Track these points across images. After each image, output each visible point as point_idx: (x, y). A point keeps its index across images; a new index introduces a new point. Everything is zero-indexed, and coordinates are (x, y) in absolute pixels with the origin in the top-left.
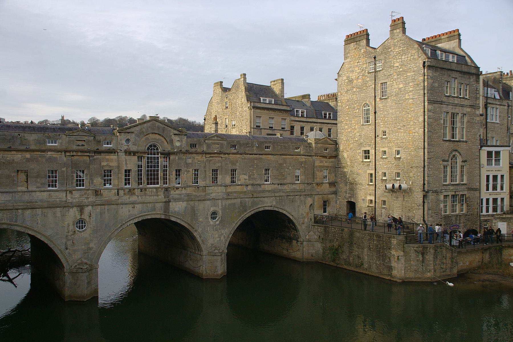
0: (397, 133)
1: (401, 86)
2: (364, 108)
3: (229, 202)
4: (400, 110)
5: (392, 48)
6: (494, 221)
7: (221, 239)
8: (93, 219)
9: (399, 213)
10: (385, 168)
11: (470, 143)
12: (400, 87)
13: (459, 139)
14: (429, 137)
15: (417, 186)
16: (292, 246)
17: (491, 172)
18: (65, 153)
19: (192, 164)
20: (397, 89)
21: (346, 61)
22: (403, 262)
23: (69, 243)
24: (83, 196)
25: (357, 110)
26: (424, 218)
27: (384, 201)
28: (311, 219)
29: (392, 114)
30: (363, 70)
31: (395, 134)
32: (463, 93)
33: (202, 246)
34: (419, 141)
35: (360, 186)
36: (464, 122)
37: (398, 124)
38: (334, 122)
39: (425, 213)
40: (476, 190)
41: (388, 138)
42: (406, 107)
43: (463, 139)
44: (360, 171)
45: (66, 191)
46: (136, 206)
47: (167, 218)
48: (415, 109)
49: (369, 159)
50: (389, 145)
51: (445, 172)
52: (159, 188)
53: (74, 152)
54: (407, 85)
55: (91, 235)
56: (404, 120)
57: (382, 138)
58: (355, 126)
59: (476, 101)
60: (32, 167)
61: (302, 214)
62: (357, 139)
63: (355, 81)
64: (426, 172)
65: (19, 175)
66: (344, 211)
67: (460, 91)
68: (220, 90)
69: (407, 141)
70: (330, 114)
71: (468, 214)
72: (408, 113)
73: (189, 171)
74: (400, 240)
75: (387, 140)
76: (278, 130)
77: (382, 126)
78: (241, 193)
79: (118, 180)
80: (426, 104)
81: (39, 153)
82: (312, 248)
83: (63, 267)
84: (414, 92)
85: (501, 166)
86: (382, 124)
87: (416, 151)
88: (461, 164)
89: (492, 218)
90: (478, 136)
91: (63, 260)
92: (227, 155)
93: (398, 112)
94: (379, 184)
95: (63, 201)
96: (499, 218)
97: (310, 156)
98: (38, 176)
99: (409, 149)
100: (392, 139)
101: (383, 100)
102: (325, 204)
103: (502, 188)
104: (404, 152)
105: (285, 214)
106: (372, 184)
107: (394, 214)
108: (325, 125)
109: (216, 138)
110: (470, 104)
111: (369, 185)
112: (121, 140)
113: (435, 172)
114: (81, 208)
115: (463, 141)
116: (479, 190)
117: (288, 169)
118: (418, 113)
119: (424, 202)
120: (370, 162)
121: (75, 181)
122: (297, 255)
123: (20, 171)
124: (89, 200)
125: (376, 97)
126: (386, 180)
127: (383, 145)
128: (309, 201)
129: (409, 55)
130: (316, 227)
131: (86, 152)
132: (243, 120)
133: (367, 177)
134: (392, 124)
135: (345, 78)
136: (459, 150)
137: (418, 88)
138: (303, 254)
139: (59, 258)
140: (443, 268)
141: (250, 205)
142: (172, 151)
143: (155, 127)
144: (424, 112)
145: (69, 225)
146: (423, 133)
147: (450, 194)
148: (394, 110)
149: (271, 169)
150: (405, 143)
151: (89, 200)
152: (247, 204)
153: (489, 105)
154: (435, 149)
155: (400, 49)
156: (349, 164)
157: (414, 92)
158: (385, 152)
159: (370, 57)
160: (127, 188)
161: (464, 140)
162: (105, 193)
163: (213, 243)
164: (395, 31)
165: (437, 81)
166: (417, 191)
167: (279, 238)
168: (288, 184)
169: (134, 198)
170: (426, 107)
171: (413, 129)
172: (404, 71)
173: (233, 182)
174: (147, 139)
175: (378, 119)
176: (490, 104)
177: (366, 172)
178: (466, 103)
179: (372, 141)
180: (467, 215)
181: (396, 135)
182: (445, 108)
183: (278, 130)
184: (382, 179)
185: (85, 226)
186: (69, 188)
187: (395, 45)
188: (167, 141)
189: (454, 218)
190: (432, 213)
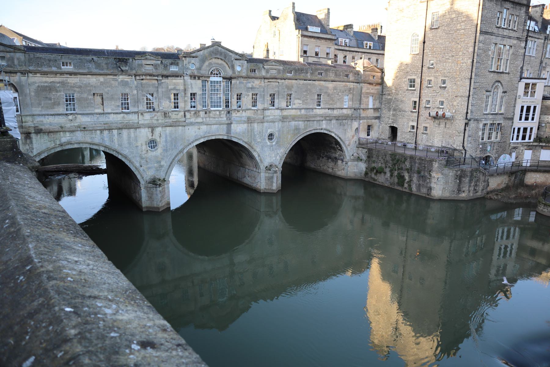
0: (445, 62)
2: (413, 38)
4: (450, 40)
6: (522, 148)
7: (277, 158)
8: (163, 139)
9: (440, 138)
10: (430, 97)
11: (511, 74)
12: (452, 17)
13: (503, 70)
14: (477, 68)
15: (460, 114)
16: (337, 165)
17: (533, 103)
18: (135, 77)
19: (251, 88)
20: (449, 20)
22: (442, 183)
23: (143, 162)
24: (153, 118)
26: (463, 143)
27: (426, 127)
28: (356, 142)
29: (442, 44)
31: (442, 64)
32: (512, 24)
34: (466, 71)
35: (403, 112)
37: (446, 54)
38: (381, 52)
39: (465, 140)
41: (435, 68)
42: (457, 38)
43: (506, 70)
44: (404, 99)
46: (201, 127)
47: (229, 139)
48: (466, 40)
49: (414, 87)
50: (435, 74)
51: (487, 102)
52: (221, 111)
53: (143, 76)
54: (460, 15)
55: (162, 154)
56: (453, 51)
57: (429, 68)
59: (523, 33)
60: (106, 90)
62: (403, 68)
64: (471, 101)
65: (95, 98)
66: (387, 133)
67: (510, 23)
69: (454, 71)
71: (501, 141)
72: (458, 44)
73: (249, 95)
74: (441, 164)
75: (433, 69)
76: (323, 58)
77: (431, 55)
80: (478, 34)
81: (112, 77)
82: (355, 168)
83: (139, 182)
84: (466, 22)
85: (535, 97)
86: (430, 53)
87: (463, 81)
88: (501, 94)
89: (521, 145)
91: (139, 177)
92: (283, 81)
93: (448, 43)
97: (358, 83)
98: (112, 98)
99: (455, 79)
100: (439, 69)
101: (434, 30)
102: (369, 128)
103: (533, 119)
104: (451, 82)
105: (333, 137)
106: (415, 111)
107: (435, 139)
109: (274, 63)
110: (517, 36)
111: (412, 112)
112: (186, 65)
113: (478, 102)
114: (153, 128)
115: (506, 73)
116: (512, 119)
117: (338, 95)
118: (468, 44)
119: (465, 130)
120: (415, 90)
121: (145, 103)
122: (341, 173)
123: (96, 94)
126: (429, 108)
127: (430, 74)
128: (355, 124)
130: (360, 149)
131: (154, 76)
133: (411, 105)
134: (441, 54)
136: (501, 81)
138: (347, 172)
139: (132, 170)
141: (303, 128)
142: (233, 76)
143: (218, 52)
144: (475, 42)
145: (142, 145)
146: (471, 64)
147: (489, 122)
148: (444, 40)
149: (323, 94)
150: (452, 73)
153: (529, 38)
154: (480, 80)
156: (394, 91)
157: (466, 22)
158: (430, 81)
160: (192, 111)
161: (507, 71)
162: (174, 116)
163: (270, 161)
165: (491, 12)
166: (460, 119)
167: (325, 158)
168: (337, 109)
170: (477, 37)
171: (461, 59)
174: (210, 64)
175: (427, 49)
176: (530, 36)
177: (409, 99)
178: (512, 34)
179: (419, 71)
180: (500, 142)
181: (443, 65)
183: (323, 58)
184: (426, 107)
185: (156, 145)
188: (229, 66)
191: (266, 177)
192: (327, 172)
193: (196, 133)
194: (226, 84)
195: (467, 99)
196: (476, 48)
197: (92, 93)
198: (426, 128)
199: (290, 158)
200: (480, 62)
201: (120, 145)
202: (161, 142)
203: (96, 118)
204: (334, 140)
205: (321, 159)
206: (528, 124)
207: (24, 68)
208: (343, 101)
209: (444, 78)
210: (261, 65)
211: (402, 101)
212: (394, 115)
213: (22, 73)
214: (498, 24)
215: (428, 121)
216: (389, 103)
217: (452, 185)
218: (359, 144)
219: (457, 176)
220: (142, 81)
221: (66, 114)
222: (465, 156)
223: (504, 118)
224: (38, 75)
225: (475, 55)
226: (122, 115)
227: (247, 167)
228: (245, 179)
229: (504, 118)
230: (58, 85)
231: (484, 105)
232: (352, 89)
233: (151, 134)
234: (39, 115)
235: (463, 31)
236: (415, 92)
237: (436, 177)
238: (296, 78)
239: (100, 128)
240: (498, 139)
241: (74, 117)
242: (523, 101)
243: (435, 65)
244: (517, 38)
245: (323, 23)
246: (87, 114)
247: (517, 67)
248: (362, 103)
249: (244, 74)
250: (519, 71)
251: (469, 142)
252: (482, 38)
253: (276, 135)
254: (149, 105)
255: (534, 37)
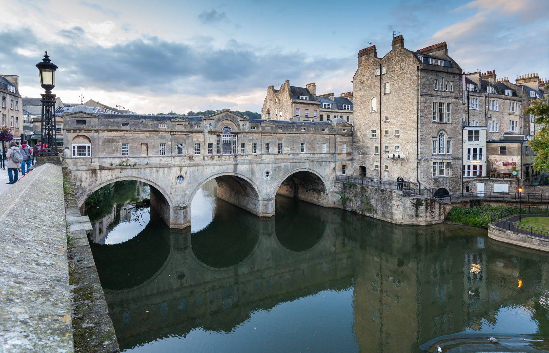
1: (400, 84)
3: (277, 165)
5: (394, 58)
6: (474, 182)
8: (188, 175)
17: (472, 146)
19: (252, 140)
21: (360, 68)
22: (401, 209)
23: (173, 191)
25: (367, 103)
26: (417, 178)
28: (334, 178)
30: (371, 74)
33: (259, 194)
36: (449, 109)
39: (418, 175)
40: (459, 159)
44: (369, 145)
45: (171, 157)
46: (215, 167)
47: (236, 175)
49: (376, 136)
58: (366, 113)
59: (459, 94)
61: (327, 174)
62: (367, 123)
63: (366, 83)
66: (358, 172)
68: (272, 92)
70: (348, 106)
71: (453, 176)
78: (285, 159)
79: (204, 151)
81: (154, 133)
82: (334, 198)
83: (169, 206)
88: (447, 140)
89: (473, 180)
90: (461, 119)
92: (275, 134)
94: (383, 154)
95: (169, 164)
96: (477, 180)
97: (333, 135)
98: (154, 147)
102: (344, 168)
108: (345, 114)
109: (268, 123)
114: (181, 168)
115: (449, 123)
116: (461, 159)
117: (317, 143)
119: (417, 167)
123: (143, 145)
124: (186, 163)
125: (382, 93)
128: (333, 165)
129: (407, 62)
130: (338, 183)
131: (183, 132)
132: (287, 111)
135: (358, 80)
137: (413, 86)
140: (432, 215)
142: (239, 131)
144: (418, 102)
147: (438, 161)
151: (186, 163)
152: (289, 167)
153: (470, 97)
155: (400, 58)
156: (361, 140)
159: (377, 65)
160: (209, 156)
161: (450, 122)
163: (266, 192)
164: (396, 45)
168: (317, 153)
169: (214, 162)
170: (419, 99)
172: (403, 73)
173: (279, 152)
174: (223, 124)
176: (471, 95)
177: (373, 146)
182: (434, 99)
184: (385, 151)
186: (173, 154)
187: (396, 56)
189: (441, 179)
190: (424, 175)
191: (263, 204)
192: (312, 202)
193: (211, 171)
194: (234, 137)
195: (416, 144)
196: (419, 106)
197: (140, 143)
198: (387, 167)
199: (286, 191)
200: (424, 116)
201: (157, 179)
202: (187, 177)
203: (142, 160)
204: (316, 177)
205: (308, 191)
206: (477, 162)
207: (97, 128)
208: (322, 148)
209: (397, 129)
210: (259, 124)
211: (367, 147)
212: (362, 158)
213: (95, 130)
214: (436, 89)
215: (388, 161)
216: (358, 149)
217: (411, 211)
218: (337, 180)
219: (414, 204)
220: (175, 136)
221: (122, 157)
222: (420, 188)
223: (453, 158)
224: (106, 132)
225: (419, 111)
226: (160, 158)
227: (250, 196)
228: (249, 205)
229: (453, 158)
230: (118, 138)
231: (432, 148)
232: (329, 139)
233: (180, 171)
234: (103, 158)
235: (408, 94)
236: (377, 140)
237: (396, 204)
238: (285, 132)
239: (144, 167)
240: (450, 175)
241: (127, 159)
242: (467, 145)
243: (389, 120)
244: (455, 97)
245: (311, 93)
246: (135, 157)
247: (458, 119)
248: (337, 149)
249: (247, 131)
250: (461, 122)
251: (422, 177)
252: (423, 99)
253: (271, 172)
254: (180, 151)
255: (475, 96)
